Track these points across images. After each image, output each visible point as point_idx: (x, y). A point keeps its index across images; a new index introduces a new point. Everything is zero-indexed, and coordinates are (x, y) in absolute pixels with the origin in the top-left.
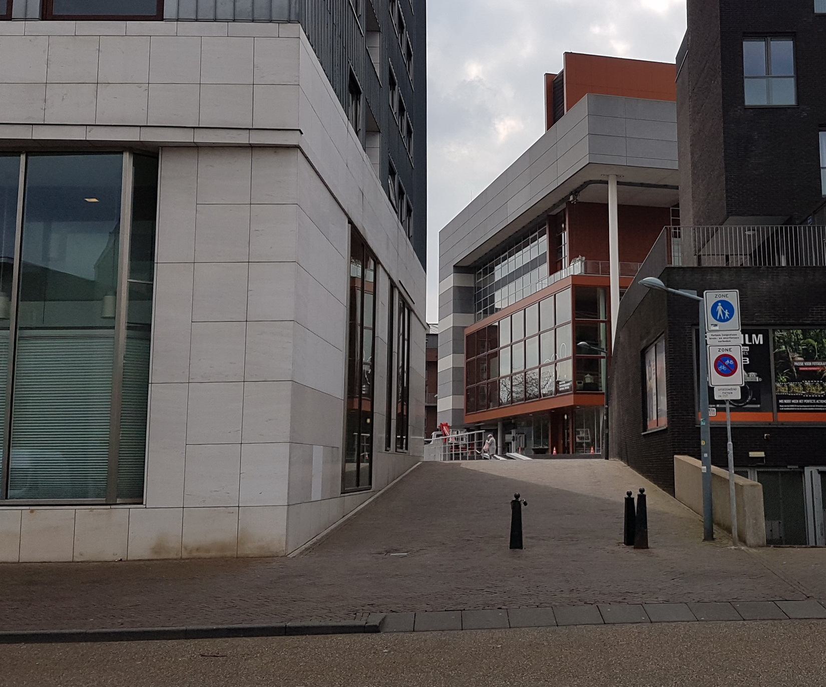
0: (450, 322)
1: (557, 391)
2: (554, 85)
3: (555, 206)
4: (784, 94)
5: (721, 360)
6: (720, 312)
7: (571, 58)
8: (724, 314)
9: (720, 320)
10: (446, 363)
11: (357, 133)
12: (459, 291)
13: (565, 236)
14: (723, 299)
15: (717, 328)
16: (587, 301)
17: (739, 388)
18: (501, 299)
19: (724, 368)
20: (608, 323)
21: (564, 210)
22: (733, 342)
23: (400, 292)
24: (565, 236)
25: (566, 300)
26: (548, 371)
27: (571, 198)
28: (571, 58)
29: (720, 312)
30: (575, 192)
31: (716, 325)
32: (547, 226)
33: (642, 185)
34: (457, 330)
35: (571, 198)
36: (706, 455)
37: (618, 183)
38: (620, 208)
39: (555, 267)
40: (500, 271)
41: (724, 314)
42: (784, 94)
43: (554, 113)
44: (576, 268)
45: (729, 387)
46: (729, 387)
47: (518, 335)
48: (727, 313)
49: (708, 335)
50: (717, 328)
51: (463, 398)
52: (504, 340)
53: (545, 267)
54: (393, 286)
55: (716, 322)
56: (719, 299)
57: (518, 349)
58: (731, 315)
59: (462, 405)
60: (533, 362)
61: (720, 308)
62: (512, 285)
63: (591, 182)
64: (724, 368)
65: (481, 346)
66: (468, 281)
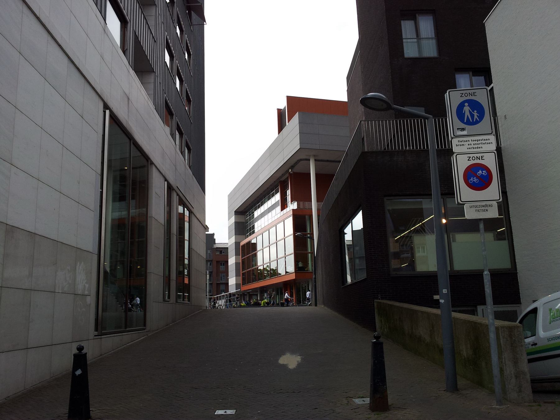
0: (233, 240)
1: (286, 272)
2: (280, 113)
3: (283, 175)
4: (430, 50)
5: (471, 171)
6: (467, 114)
7: (291, 100)
8: (472, 116)
9: (468, 123)
10: (232, 261)
11: (124, 52)
12: (237, 224)
13: (289, 192)
14: (468, 98)
15: (465, 133)
16: (301, 222)
17: (495, 204)
18: (258, 226)
19: (475, 180)
20: (312, 238)
21: (288, 178)
22: (486, 148)
23: (178, 195)
24: (289, 192)
25: (290, 222)
26: (281, 262)
27: (290, 171)
28: (291, 100)
29: (467, 114)
30: (292, 167)
31: (463, 129)
32: (279, 187)
33: (328, 161)
34: (237, 244)
35: (290, 171)
36: (445, 291)
37: (315, 160)
38: (317, 176)
39: (284, 206)
40: (257, 213)
41: (472, 116)
42: (430, 50)
43: (281, 126)
44: (294, 206)
45: (484, 203)
46: (484, 203)
47: (266, 243)
48: (476, 114)
49: (455, 142)
50: (465, 133)
51: (240, 278)
52: (259, 247)
53: (279, 208)
54: (170, 188)
55: (463, 126)
56: (465, 98)
57: (266, 250)
58: (481, 117)
59: (240, 282)
60: (274, 257)
61: (467, 109)
62: (263, 219)
63: (301, 160)
64: (475, 180)
65: (248, 252)
66: (242, 219)
